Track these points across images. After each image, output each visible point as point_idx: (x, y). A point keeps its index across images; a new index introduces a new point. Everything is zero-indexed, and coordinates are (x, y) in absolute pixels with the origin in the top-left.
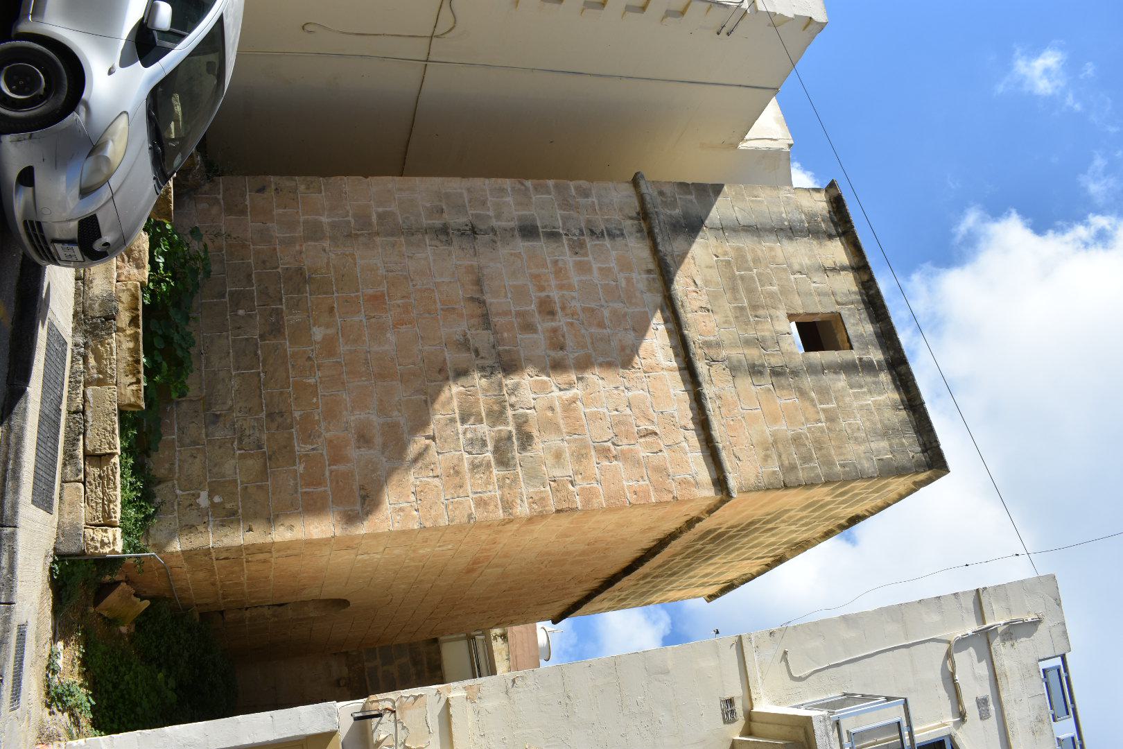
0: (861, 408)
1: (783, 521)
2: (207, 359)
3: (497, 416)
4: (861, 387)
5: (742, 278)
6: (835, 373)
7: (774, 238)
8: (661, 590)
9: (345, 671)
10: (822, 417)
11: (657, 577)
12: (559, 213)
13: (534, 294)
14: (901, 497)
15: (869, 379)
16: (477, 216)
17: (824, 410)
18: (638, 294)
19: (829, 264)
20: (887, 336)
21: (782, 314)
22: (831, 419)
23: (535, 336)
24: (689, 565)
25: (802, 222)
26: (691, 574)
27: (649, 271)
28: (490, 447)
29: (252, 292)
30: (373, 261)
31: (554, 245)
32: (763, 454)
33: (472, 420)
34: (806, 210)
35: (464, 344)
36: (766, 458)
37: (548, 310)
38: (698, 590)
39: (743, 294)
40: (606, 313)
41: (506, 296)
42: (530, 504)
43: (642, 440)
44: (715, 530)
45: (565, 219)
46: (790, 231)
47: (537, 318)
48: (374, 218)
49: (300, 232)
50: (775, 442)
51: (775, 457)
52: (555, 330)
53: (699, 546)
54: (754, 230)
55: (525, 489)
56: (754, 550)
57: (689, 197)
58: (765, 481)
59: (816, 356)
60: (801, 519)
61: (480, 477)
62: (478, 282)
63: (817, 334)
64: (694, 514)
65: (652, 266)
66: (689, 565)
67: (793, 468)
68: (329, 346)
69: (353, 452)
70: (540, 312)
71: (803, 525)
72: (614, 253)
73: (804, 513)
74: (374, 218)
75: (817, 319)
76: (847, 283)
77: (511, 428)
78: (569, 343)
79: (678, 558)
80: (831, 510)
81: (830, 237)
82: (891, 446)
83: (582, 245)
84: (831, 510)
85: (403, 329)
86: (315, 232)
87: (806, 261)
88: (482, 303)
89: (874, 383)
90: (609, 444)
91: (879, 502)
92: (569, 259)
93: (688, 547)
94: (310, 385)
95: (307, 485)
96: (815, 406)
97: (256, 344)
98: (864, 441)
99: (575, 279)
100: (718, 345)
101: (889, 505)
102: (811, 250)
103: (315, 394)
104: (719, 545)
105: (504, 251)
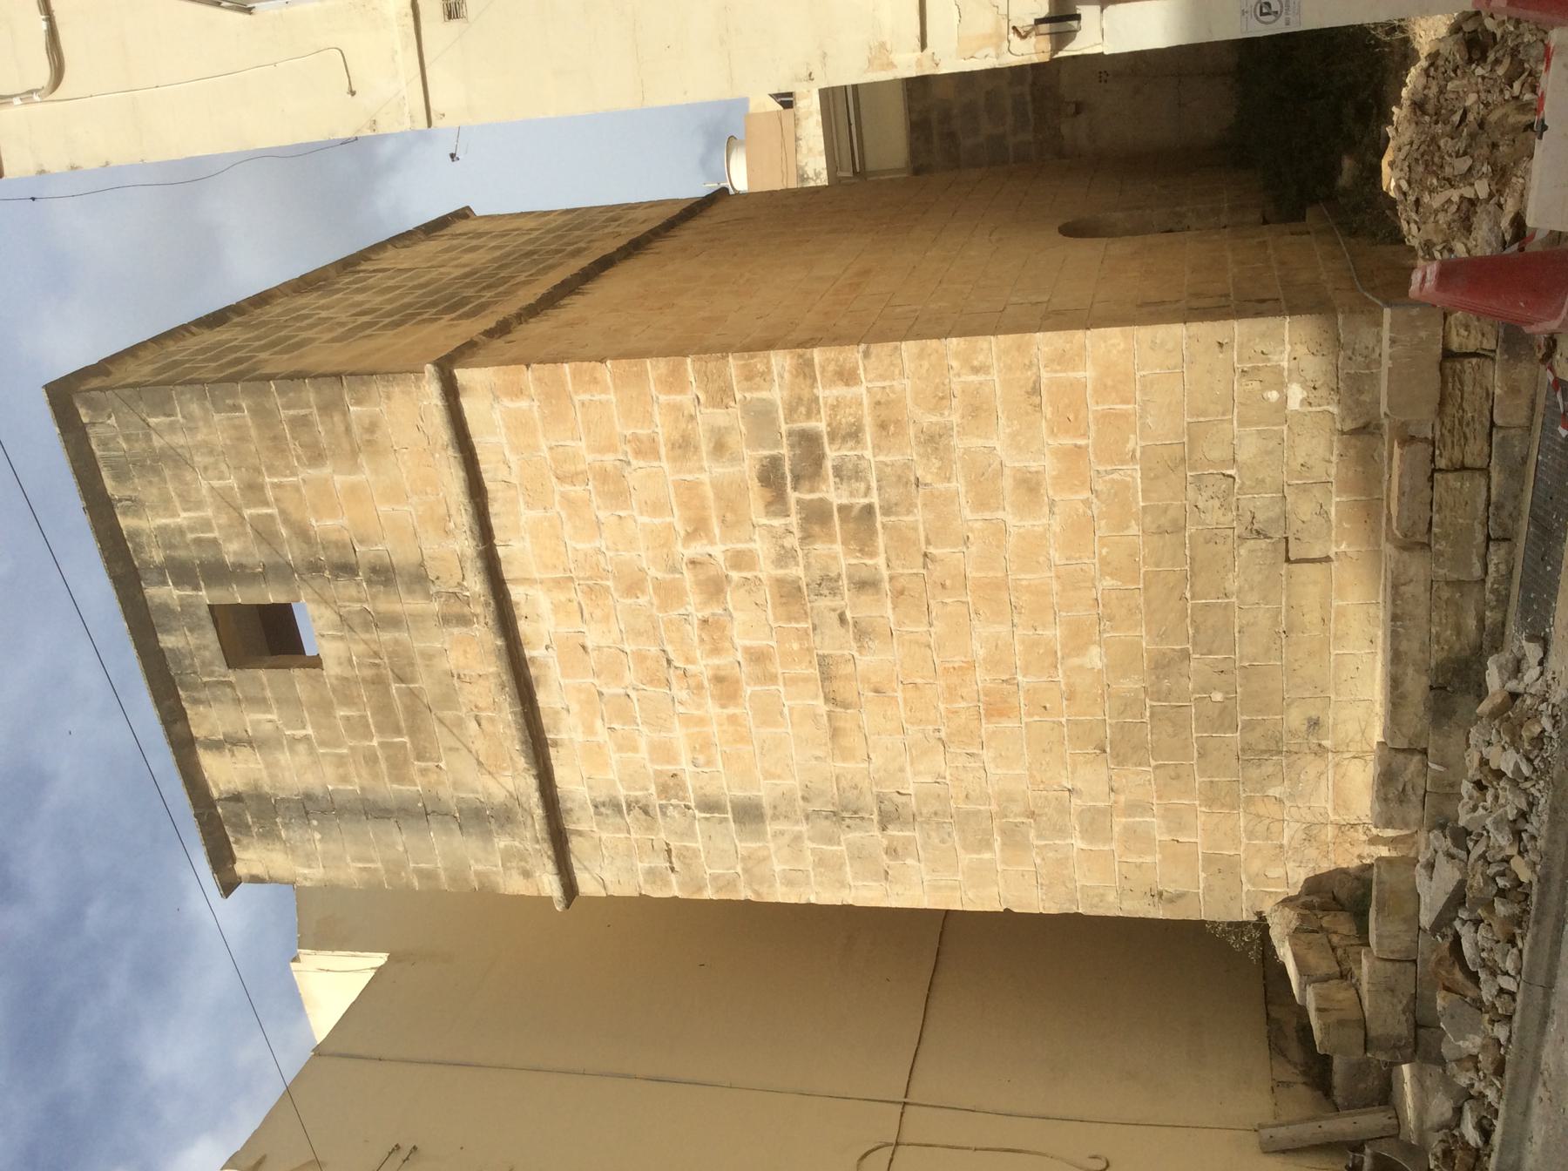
0: (199, 505)
1: (342, 324)
2: (1276, 622)
3: (816, 516)
4: (198, 541)
5: (398, 731)
6: (242, 566)
7: (337, 798)
8: (548, 232)
9: (1065, 129)
10: (270, 494)
11: (557, 252)
12: (698, 844)
13: (744, 710)
14: (132, 352)
15: (181, 554)
16: (831, 840)
17: (266, 504)
18: (574, 707)
19: (243, 753)
20: (143, 623)
21: (332, 669)
22: (253, 489)
23: (748, 643)
24: (501, 267)
25: (286, 825)
26: (498, 253)
27: (556, 744)
28: (828, 464)
29: (1199, 728)
30: (1004, 769)
31: (708, 790)
32: (378, 435)
33: (855, 512)
34: (278, 846)
35: (862, 633)
36: (372, 427)
37: (725, 686)
38: (486, 227)
39: (398, 704)
40: (630, 677)
41: (791, 709)
42: (769, 370)
43: (581, 467)
44: (460, 317)
45: (689, 833)
46: (311, 808)
47: (744, 673)
48: (997, 845)
49: (1119, 822)
50: (354, 453)
51: (356, 429)
52: (716, 651)
53: (488, 294)
54: (372, 811)
55: (776, 394)
56: (391, 283)
57: (480, 867)
58: (378, 388)
59: (273, 596)
60: (312, 326)
61: (845, 418)
62: (835, 733)
63: (268, 637)
64: (498, 343)
65: (552, 751)
66: (501, 267)
67: (326, 408)
68: (1078, 639)
69: (1046, 465)
70: (737, 681)
71: (306, 317)
72: (611, 776)
73: (304, 335)
74: (997, 845)
75: (270, 659)
76: (206, 720)
77: (792, 496)
78: (693, 632)
79: (522, 278)
80: (258, 338)
81: (236, 798)
82: (148, 438)
83: (664, 790)
84: (258, 338)
85: (958, 661)
86: (1095, 823)
87: (284, 757)
88: (830, 699)
89: (171, 546)
90: (634, 463)
91: (172, 346)
92: (684, 766)
93: (506, 293)
94: (1111, 575)
95: (1124, 416)
96: (282, 512)
97: (1195, 644)
98: (197, 447)
99: (679, 736)
100: (446, 620)
101: (156, 340)
102: (272, 776)
103: (1104, 562)
104: (453, 295)
105: (792, 783)
